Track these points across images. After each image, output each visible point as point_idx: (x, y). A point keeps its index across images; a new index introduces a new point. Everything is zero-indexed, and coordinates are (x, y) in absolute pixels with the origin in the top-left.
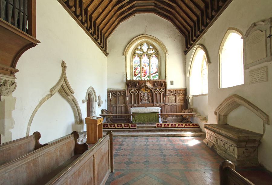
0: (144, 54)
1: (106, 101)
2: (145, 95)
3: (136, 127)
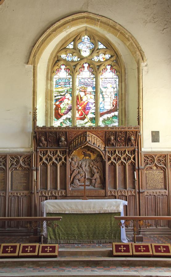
0: (82, 62)
2: (83, 166)
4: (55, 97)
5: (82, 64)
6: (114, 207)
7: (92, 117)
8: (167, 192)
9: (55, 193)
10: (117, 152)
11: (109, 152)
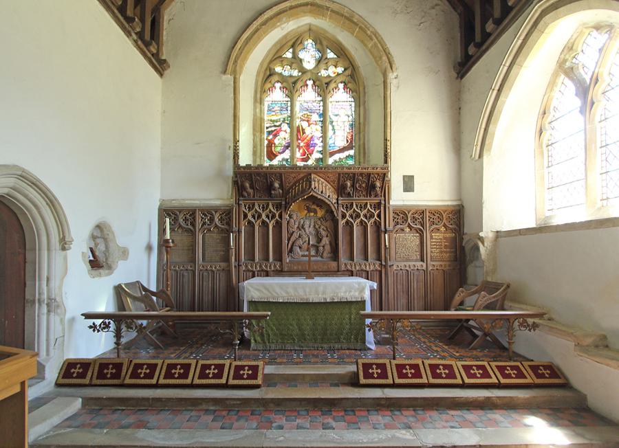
0: (305, 78)
1: (149, 248)
2: (306, 226)
3: (259, 381)
4: (267, 128)
5: (304, 81)
6: (355, 291)
7: (318, 157)
8: (424, 265)
9: (252, 267)
10: (354, 206)
11: (343, 206)
